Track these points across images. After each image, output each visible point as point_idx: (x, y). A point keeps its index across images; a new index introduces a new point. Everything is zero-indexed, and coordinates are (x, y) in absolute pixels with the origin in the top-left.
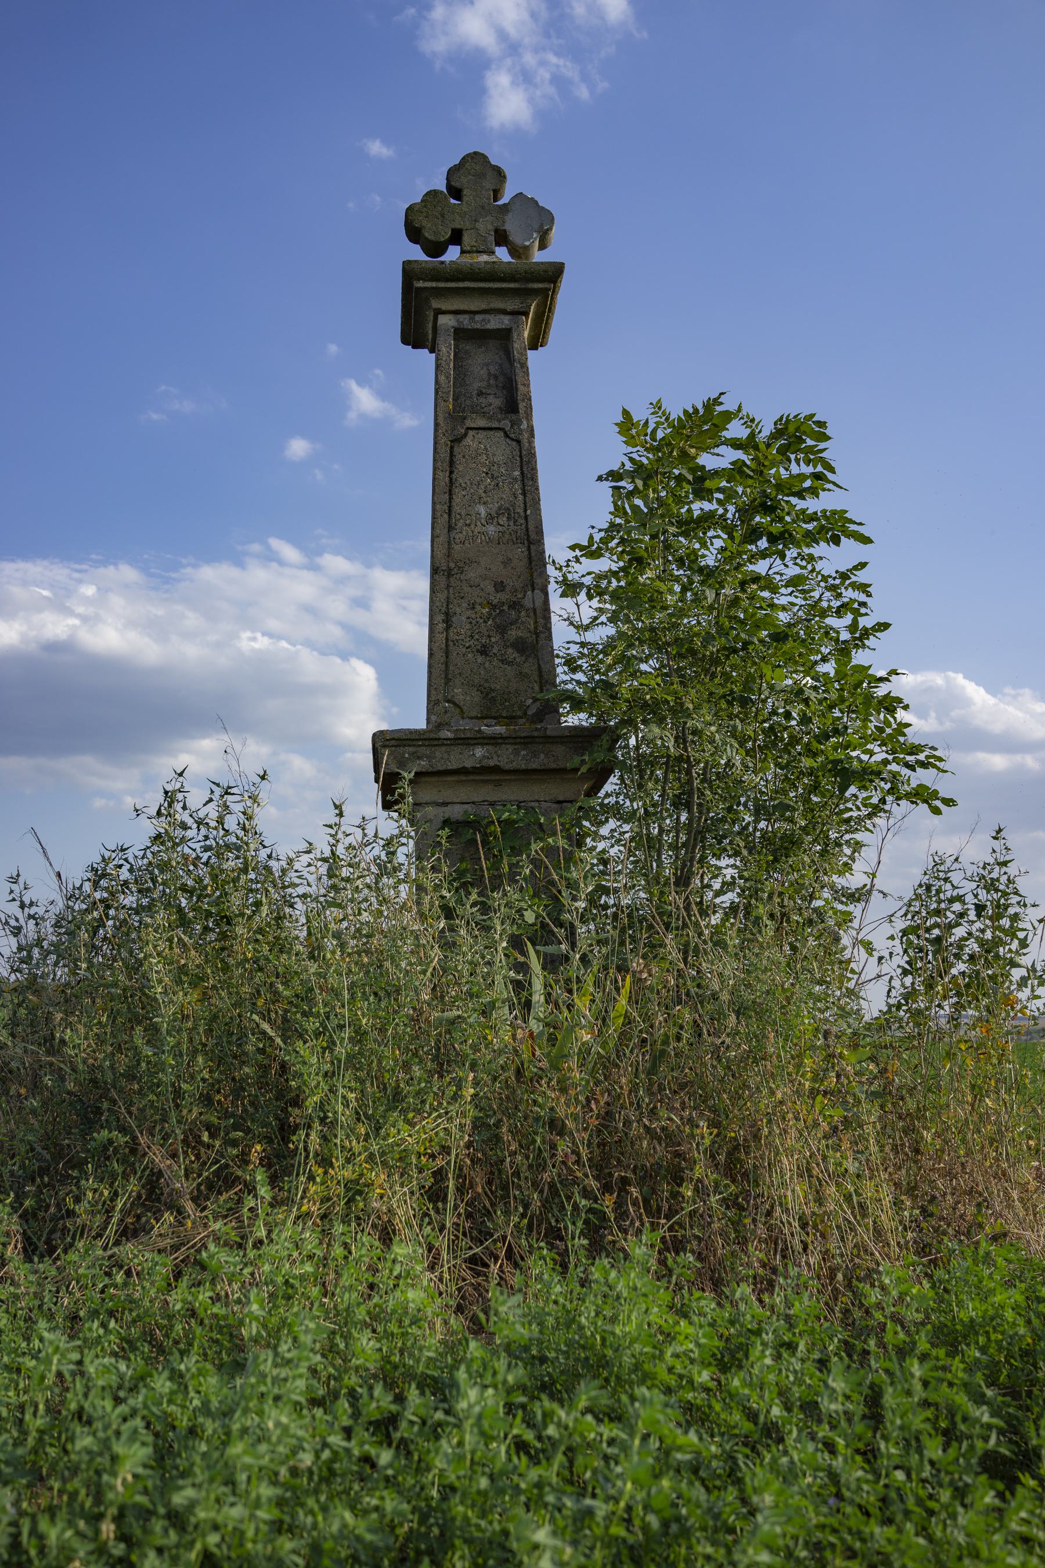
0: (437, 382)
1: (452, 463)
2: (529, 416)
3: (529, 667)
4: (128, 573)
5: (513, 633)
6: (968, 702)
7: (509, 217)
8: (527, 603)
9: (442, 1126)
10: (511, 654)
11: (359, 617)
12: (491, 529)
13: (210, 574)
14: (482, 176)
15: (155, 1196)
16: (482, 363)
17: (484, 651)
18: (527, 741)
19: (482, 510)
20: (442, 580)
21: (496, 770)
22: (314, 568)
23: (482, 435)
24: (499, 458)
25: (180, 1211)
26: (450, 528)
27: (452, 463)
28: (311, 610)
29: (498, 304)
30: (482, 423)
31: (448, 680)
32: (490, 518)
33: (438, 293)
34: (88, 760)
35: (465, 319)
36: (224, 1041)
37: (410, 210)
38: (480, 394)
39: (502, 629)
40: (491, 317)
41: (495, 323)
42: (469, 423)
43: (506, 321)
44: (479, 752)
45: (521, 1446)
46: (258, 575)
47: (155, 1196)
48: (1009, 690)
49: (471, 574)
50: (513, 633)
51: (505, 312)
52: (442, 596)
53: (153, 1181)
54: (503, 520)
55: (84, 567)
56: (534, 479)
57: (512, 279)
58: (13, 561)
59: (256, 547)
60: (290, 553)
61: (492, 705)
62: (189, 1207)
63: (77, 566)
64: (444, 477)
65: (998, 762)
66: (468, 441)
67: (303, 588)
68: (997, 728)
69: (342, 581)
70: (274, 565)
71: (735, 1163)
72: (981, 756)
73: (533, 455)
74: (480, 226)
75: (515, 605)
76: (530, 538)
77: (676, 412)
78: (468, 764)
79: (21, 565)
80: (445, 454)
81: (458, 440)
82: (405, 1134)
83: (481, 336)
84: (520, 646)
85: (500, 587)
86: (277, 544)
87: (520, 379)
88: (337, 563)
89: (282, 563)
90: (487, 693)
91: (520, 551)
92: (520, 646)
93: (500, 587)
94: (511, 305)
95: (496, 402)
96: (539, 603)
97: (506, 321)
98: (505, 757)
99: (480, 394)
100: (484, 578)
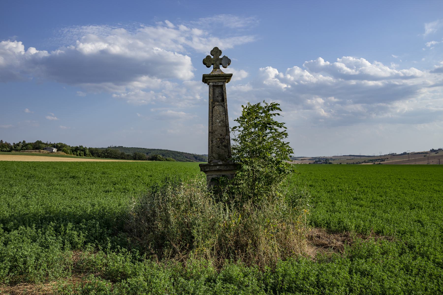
0: (209, 96)
1: (212, 112)
2: (226, 102)
3: (226, 150)
4: (123, 30)
5: (224, 144)
6: (365, 65)
7: (222, 61)
8: (226, 138)
9: (213, 240)
10: (223, 147)
11: (189, 43)
12: (220, 124)
13: (148, 30)
14: (217, 52)
15: (175, 252)
16: (217, 91)
17: (218, 147)
18: (226, 165)
19: (218, 121)
20: (211, 134)
21: (221, 170)
22: (177, 29)
23: (218, 106)
24: (221, 111)
25: (178, 253)
26: (212, 124)
27: (212, 112)
28: (175, 41)
30: (217, 104)
31: (212, 153)
32: (219, 122)
33: (209, 79)
34: (110, 84)
36: (181, 225)
37: (204, 60)
38: (217, 97)
39: (222, 143)
41: (220, 84)
43: (222, 83)
44: (218, 167)
45: (222, 287)
46: (161, 31)
47: (175, 252)
48: (376, 62)
49: (216, 133)
50: (224, 144)
52: (211, 137)
53: (174, 249)
54: (222, 123)
56: (227, 114)
58: (96, 26)
59: (161, 23)
60: (170, 25)
61: (220, 157)
62: (180, 253)
64: (211, 114)
65: (371, 83)
66: (215, 107)
67: (173, 34)
68: (372, 74)
69: (185, 32)
70: (166, 28)
71: (255, 245)
72: (366, 81)
73: (227, 110)
75: (224, 139)
76: (226, 126)
77: (252, 105)
79: (98, 27)
80: (211, 110)
81: (213, 107)
82: (208, 242)
83: (217, 86)
84: (225, 146)
85: (221, 135)
86: (167, 22)
87: (225, 95)
88: (183, 27)
89: (168, 28)
90: (219, 155)
91: (225, 128)
92: (225, 146)
93: (221, 135)
94: (223, 81)
95: (220, 98)
96: (228, 138)
97: (222, 83)
98: (222, 168)
99: (217, 97)
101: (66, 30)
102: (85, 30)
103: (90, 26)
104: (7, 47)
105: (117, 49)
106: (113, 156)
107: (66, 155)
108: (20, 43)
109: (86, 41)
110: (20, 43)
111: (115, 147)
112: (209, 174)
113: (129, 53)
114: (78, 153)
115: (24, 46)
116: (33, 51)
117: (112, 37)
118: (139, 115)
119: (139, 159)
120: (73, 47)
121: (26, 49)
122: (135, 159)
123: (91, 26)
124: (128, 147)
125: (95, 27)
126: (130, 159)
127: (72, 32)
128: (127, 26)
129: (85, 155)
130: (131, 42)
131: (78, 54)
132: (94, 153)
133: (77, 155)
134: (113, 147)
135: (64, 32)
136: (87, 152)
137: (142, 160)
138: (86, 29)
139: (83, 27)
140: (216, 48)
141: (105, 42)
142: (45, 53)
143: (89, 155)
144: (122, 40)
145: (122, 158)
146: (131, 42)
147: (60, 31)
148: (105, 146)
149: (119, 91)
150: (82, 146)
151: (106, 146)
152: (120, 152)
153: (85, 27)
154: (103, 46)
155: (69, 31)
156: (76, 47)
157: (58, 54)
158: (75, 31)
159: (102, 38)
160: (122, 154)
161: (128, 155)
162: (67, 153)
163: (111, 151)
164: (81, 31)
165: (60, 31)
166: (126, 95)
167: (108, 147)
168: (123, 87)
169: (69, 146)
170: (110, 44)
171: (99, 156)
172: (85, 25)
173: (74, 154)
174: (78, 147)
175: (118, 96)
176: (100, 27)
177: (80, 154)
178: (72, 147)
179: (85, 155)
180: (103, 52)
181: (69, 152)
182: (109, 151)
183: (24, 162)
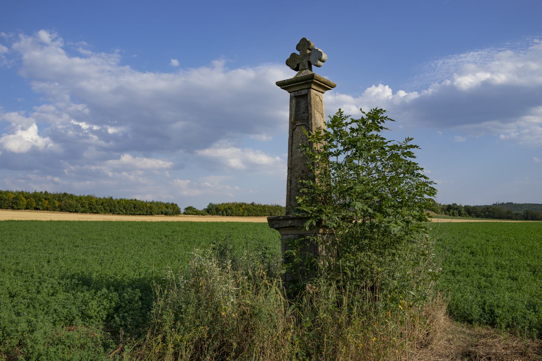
4: (509, 53)
14: (304, 45)
21: (294, 226)
29: (303, 87)
30: (300, 124)
34: (496, 123)
35: (296, 93)
40: (302, 91)
42: (297, 124)
44: (290, 222)
49: (296, 169)
51: (305, 89)
55: (503, 49)
57: (302, 81)
58: (477, 51)
63: (500, 49)
66: (296, 130)
74: (304, 61)
78: (287, 225)
79: (480, 52)
81: (294, 130)
93: (303, 172)
94: (306, 87)
97: (306, 91)
99: (304, 113)
100: (299, 169)
101: (440, 62)
102: (463, 59)
103: (470, 52)
104: (374, 94)
105: (501, 78)
106: (496, 215)
107: (436, 215)
108: (387, 87)
109: (461, 73)
110: (387, 87)
111: (503, 204)
112: (283, 233)
113: (518, 81)
114: (451, 213)
115: (392, 89)
116: (402, 93)
117: (497, 63)
118: (536, 160)
119: (532, 219)
120: (448, 82)
121: (394, 93)
122: (526, 219)
123: (472, 53)
124: (521, 203)
125: (477, 53)
126: (520, 219)
127: (448, 63)
128: (518, 43)
129: (459, 215)
130: (520, 65)
131: (453, 88)
132: (470, 212)
133: (450, 215)
134: (500, 204)
135: (439, 65)
136: (463, 211)
137: (536, 219)
138: (465, 57)
139: (461, 55)
140: (304, 40)
141: (487, 70)
142: (414, 95)
143: (465, 214)
144: (510, 66)
145: (509, 218)
146: (520, 65)
147: (433, 65)
148: (489, 202)
149: (509, 131)
150: (455, 204)
151: (490, 203)
152: (505, 210)
153: (464, 55)
154: (484, 76)
155: (444, 63)
156: (453, 81)
157: (430, 93)
158: (451, 61)
159: (483, 66)
160: (508, 212)
161: (517, 214)
162: (437, 213)
163: (493, 209)
164: (459, 60)
165: (433, 65)
166: (517, 134)
167: (494, 204)
168: (512, 125)
169: (440, 204)
170: (492, 73)
171: (478, 216)
172: (464, 53)
173: (446, 214)
174: (450, 206)
175: (508, 136)
176: (483, 52)
177: (453, 213)
178: (444, 205)
179: (460, 215)
180: (486, 84)
181: (440, 211)
182: (491, 209)
183: (41, 222)
